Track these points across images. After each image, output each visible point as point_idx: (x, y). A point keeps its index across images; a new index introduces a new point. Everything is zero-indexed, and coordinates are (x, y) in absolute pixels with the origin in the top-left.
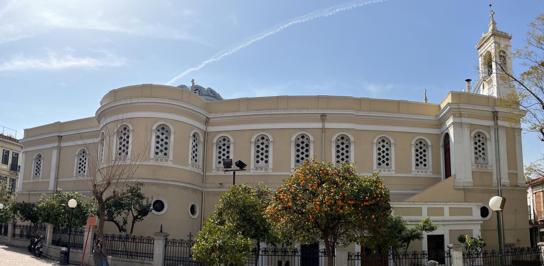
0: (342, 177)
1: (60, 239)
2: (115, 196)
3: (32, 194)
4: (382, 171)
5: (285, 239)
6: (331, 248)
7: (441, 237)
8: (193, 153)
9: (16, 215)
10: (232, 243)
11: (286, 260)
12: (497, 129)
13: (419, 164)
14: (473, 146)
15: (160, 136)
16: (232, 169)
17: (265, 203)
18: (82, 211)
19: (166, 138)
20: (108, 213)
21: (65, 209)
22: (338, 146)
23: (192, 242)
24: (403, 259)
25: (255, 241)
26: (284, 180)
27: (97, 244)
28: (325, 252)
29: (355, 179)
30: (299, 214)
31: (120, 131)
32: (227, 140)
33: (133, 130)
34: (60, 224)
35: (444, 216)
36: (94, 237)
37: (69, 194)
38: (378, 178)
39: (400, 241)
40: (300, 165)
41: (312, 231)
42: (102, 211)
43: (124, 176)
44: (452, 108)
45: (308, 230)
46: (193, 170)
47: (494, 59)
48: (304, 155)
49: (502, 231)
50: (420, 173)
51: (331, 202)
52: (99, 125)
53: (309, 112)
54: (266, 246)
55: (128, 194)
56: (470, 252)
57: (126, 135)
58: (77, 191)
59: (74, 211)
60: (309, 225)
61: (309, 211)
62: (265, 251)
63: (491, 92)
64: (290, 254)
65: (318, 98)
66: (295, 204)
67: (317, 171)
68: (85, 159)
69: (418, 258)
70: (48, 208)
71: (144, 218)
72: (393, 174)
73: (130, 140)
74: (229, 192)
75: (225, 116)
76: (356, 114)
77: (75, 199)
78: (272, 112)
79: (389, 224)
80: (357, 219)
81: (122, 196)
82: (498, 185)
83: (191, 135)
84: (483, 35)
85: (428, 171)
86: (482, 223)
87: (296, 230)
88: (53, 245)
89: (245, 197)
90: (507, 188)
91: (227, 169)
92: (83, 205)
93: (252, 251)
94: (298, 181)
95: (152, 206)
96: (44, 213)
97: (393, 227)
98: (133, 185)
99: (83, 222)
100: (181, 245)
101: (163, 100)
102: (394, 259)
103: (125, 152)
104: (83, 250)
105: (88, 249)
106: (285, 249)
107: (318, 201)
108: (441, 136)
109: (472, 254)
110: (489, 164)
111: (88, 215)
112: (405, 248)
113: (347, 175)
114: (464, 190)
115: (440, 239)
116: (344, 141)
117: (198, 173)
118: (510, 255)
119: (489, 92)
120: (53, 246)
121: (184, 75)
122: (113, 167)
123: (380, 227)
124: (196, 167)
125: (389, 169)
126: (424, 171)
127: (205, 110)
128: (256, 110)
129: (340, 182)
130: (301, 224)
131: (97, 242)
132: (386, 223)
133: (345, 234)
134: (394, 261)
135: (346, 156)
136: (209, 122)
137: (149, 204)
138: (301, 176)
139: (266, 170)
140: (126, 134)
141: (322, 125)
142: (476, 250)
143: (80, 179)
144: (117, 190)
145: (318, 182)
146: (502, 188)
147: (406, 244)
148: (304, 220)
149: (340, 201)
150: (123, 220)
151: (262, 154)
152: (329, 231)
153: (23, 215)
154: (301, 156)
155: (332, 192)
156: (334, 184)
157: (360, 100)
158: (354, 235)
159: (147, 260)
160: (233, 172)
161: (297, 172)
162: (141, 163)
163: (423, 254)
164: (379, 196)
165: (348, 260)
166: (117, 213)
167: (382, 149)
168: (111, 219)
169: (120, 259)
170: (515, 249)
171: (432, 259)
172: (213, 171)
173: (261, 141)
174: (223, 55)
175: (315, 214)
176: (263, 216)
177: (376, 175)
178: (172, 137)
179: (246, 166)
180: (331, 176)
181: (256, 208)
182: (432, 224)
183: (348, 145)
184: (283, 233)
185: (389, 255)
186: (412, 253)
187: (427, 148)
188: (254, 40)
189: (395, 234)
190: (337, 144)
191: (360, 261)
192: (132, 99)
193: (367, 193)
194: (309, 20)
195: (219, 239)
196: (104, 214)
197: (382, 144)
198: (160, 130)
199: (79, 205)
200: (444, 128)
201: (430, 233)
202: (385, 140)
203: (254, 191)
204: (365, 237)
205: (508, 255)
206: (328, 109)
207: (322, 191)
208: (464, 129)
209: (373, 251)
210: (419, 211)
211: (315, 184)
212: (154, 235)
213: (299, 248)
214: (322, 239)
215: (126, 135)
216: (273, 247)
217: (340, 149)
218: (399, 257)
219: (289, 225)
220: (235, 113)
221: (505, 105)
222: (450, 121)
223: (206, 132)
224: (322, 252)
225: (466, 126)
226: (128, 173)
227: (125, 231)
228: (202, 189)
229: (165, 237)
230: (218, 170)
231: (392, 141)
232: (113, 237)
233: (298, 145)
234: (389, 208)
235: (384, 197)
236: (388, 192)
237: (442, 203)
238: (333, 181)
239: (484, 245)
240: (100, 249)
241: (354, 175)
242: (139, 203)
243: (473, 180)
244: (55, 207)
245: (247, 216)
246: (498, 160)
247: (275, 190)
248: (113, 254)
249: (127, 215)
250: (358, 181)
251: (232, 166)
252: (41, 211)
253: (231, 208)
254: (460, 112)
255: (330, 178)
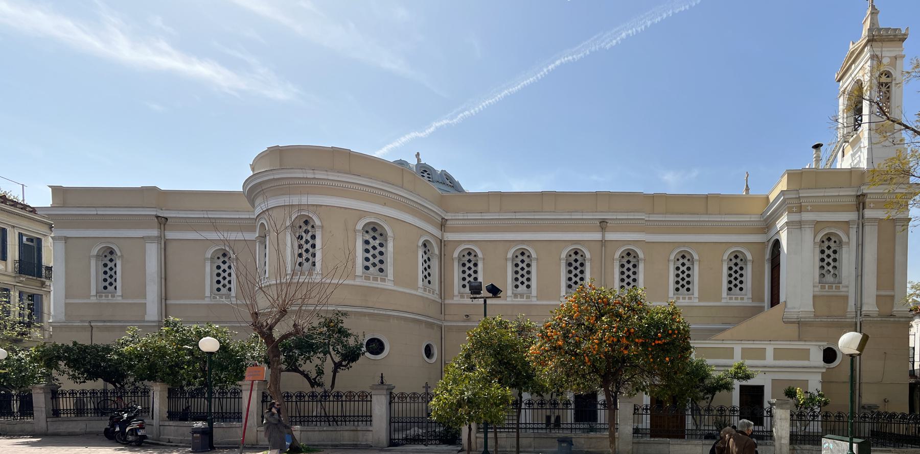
0: (628, 307)
1: (188, 408)
2: (297, 332)
3: (98, 327)
4: (681, 298)
5: (554, 388)
6: (612, 399)
7: (760, 389)
8: (424, 271)
9: (54, 371)
10: (485, 395)
11: (556, 415)
12: (863, 224)
13: (733, 288)
14: (818, 256)
15: (371, 241)
16: (482, 295)
17: (527, 342)
18: (232, 356)
19: (381, 245)
20: (286, 360)
21: (193, 355)
22: (622, 266)
23: (429, 396)
24: (705, 415)
25: (516, 391)
26: (552, 312)
27: (270, 410)
28: (604, 404)
29: (644, 310)
30: (572, 355)
31: (298, 226)
32: (473, 254)
33: (322, 227)
34: (184, 383)
35: (765, 359)
36: (263, 399)
37: (198, 328)
38: (675, 308)
39: (701, 391)
40: (573, 292)
41: (588, 377)
42: (275, 356)
43: (311, 301)
44: (788, 198)
45: (584, 376)
46: (426, 296)
47: (867, 95)
48: (578, 278)
49: (858, 384)
50: (734, 301)
51: (613, 340)
52: (253, 209)
53: (584, 217)
54: (530, 397)
55: (322, 328)
56: (801, 412)
57: (310, 234)
58: (216, 323)
59: (213, 358)
60: (584, 370)
61: (584, 351)
62: (529, 404)
63: (856, 162)
64: (561, 406)
65: (597, 196)
66: (567, 342)
67: (595, 299)
68: (230, 267)
69: (725, 416)
70: (150, 354)
71: (353, 364)
72: (695, 302)
73: (318, 242)
74: (479, 327)
75: (469, 218)
76: (648, 219)
77: (215, 337)
78: (534, 215)
79: (688, 370)
80: (646, 362)
81: (311, 332)
82: (856, 315)
83: (420, 243)
84: (851, 46)
85: (745, 297)
86: (823, 372)
87: (568, 376)
88: (173, 420)
89: (501, 334)
90: (872, 319)
91: (475, 296)
92: (234, 345)
93: (513, 404)
94: (570, 313)
95: (364, 346)
96: (140, 364)
97: (693, 373)
98: (330, 316)
99: (237, 375)
100: (414, 400)
101: (372, 183)
102: (693, 415)
103: (310, 262)
104: (242, 422)
105: (253, 419)
106: (554, 401)
107: (597, 339)
108: (768, 245)
109: (804, 416)
110: (843, 282)
111: (246, 364)
112: (709, 401)
113: (634, 304)
114: (799, 323)
115: (759, 391)
116: (631, 258)
117: (434, 301)
118: (869, 422)
119: (853, 161)
120: (171, 423)
121: (403, 143)
122: (289, 285)
123: (676, 373)
124: (429, 292)
125: (691, 296)
126: (739, 297)
127: (438, 206)
128: (512, 212)
129: (624, 314)
130: (574, 369)
131: (270, 406)
132: (684, 368)
133: (631, 381)
134: (693, 417)
135: (634, 279)
136: (446, 226)
137: (359, 343)
138: (574, 306)
139: (528, 297)
140: (309, 231)
141: (601, 235)
142: (812, 410)
143: (222, 303)
144: (301, 322)
145: (596, 313)
146: (864, 319)
147: (709, 396)
148: (578, 363)
149: (625, 339)
150: (317, 368)
151: (522, 276)
152: (610, 377)
153: (78, 369)
154: (574, 279)
155: (614, 327)
156: (617, 317)
157: (653, 198)
158: (641, 383)
159: (362, 426)
160: (483, 299)
161: (569, 301)
162: (340, 282)
163: (733, 410)
164: (676, 332)
165: (634, 414)
166: (305, 359)
167: (682, 268)
168: (293, 367)
169: (317, 428)
170: (879, 414)
171: (745, 418)
172: (455, 299)
173: (520, 258)
174: (461, 115)
175: (592, 355)
176: (526, 358)
177: (672, 305)
178: (390, 245)
179: (502, 291)
180: (613, 306)
181: (516, 348)
182: (748, 371)
183: (636, 263)
184: (551, 380)
185: (687, 410)
186: (717, 409)
187: (746, 265)
188: (506, 92)
189: (695, 382)
190: (621, 263)
191: (649, 416)
192: (316, 172)
193: (660, 329)
194: (583, 57)
195: (468, 389)
196: (279, 360)
197: (681, 261)
198: (370, 231)
199: (224, 348)
200: (773, 232)
201: (744, 383)
202: (686, 255)
203: (513, 326)
204: (656, 385)
205: (865, 422)
206: (610, 212)
207: (601, 326)
208: (805, 230)
209: (666, 403)
210: (729, 353)
211: (592, 316)
212: (370, 389)
213: (572, 399)
214: (602, 388)
215: (310, 234)
216: (539, 398)
217: (625, 270)
218: (700, 413)
219: (559, 370)
220: (483, 214)
221: (880, 180)
222: (784, 220)
223: (443, 241)
224: (601, 404)
225: (808, 226)
226: (318, 296)
227: (320, 385)
228: (441, 323)
229: (389, 391)
230: (462, 297)
231: (696, 257)
232: (300, 396)
233: (570, 265)
234: (688, 348)
235: (682, 333)
236: (688, 326)
237: (763, 342)
238: (616, 313)
239: (826, 403)
240: (276, 416)
241: (643, 304)
242: (342, 343)
243: (814, 309)
244: (166, 352)
245: (504, 358)
246: (860, 276)
247: (541, 325)
248: (303, 423)
249: (323, 362)
250: (648, 312)
251: (482, 292)
252: (131, 359)
253: (483, 348)
254: (801, 203)
255: (612, 309)
